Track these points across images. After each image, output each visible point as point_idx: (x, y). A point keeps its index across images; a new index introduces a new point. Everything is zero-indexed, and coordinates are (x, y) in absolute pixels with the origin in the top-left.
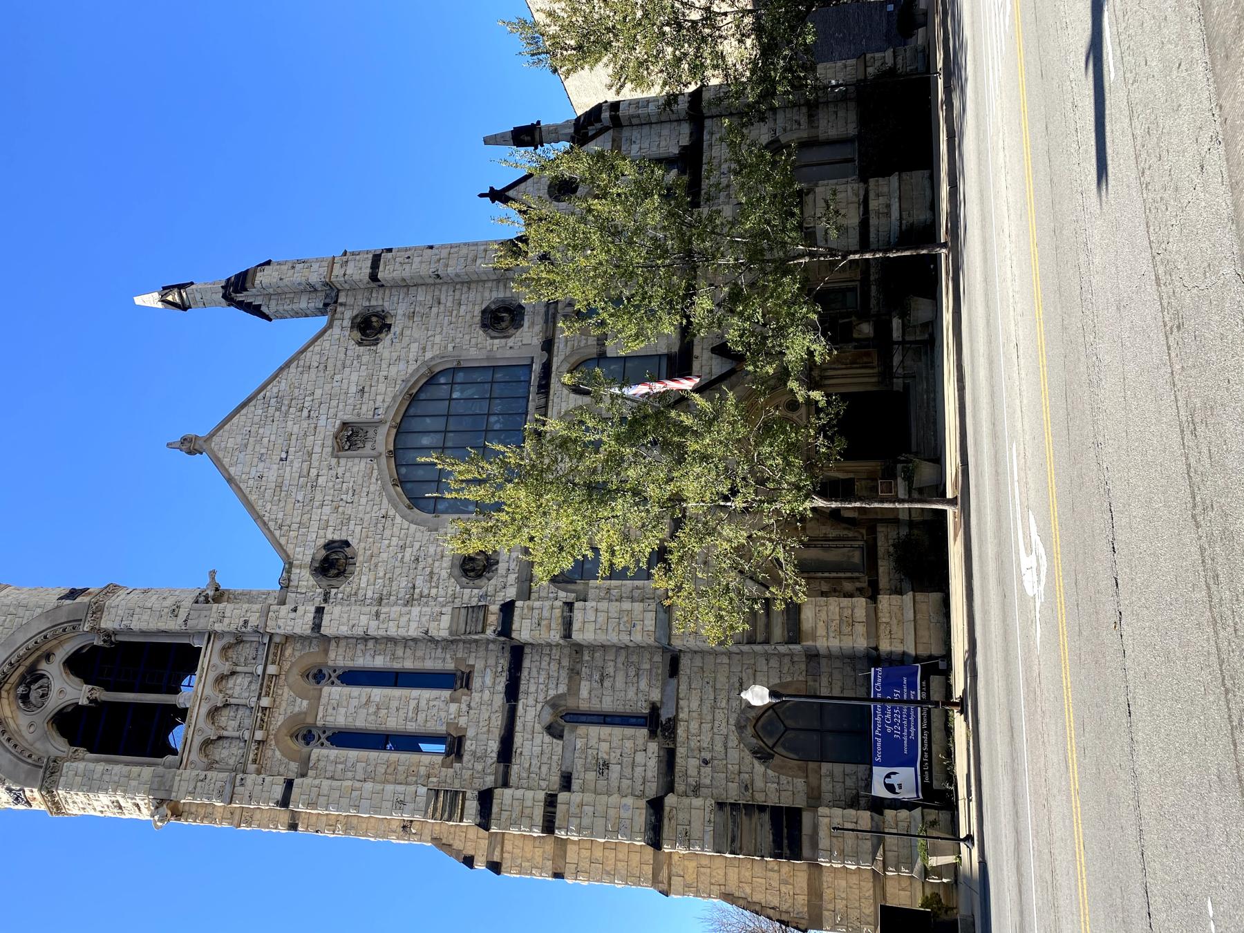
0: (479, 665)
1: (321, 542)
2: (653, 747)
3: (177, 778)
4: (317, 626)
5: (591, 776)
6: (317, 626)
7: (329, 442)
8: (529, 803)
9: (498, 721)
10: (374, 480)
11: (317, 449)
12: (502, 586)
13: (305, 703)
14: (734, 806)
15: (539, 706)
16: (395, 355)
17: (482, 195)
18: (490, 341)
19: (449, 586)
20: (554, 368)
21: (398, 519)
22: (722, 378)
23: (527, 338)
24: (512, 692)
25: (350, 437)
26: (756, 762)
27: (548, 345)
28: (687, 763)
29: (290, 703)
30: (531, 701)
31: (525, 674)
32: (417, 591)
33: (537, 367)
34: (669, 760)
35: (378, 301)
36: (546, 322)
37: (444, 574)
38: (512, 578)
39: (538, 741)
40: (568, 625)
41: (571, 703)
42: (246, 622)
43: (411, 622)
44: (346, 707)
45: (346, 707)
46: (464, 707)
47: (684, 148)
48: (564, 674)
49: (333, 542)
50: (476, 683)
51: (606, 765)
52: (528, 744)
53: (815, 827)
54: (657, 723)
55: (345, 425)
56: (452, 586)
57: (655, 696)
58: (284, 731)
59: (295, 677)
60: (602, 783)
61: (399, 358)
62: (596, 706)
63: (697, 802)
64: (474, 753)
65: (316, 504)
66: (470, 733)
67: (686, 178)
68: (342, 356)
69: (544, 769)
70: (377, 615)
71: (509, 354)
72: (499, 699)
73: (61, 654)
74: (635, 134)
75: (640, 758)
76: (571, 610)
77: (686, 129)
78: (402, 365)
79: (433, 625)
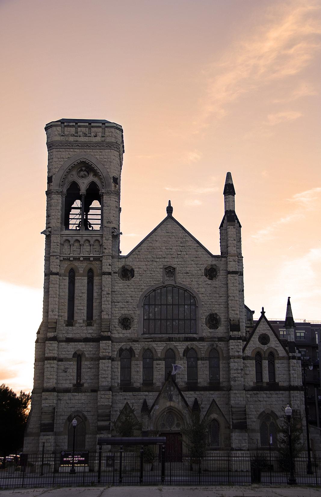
0: (94, 328)
1: (133, 267)
2: (71, 386)
3: (57, 236)
4: (104, 273)
5: (63, 367)
6: (104, 273)
7: (169, 264)
8: (53, 352)
9: (78, 336)
10: (155, 282)
11: (166, 260)
12: (118, 333)
13: (82, 272)
14: (54, 413)
15: (82, 349)
16: (200, 283)
17: (263, 308)
18: (205, 317)
19: (118, 313)
20: (194, 342)
21: (141, 293)
22: (185, 402)
23: (205, 331)
24: (86, 340)
25: (170, 271)
26: (67, 417)
27: (202, 339)
28: (66, 397)
29: (82, 267)
30: (84, 346)
31: (91, 343)
32: (117, 304)
33: (195, 335)
34: (67, 391)
35: (221, 274)
36: (211, 338)
37: (123, 312)
38: (121, 335)
39: (72, 350)
40: (104, 358)
41: (83, 359)
42: (106, 249)
43: (106, 306)
44: (81, 284)
45: (81, 284)
46: (82, 325)
47: (278, 384)
48: (91, 356)
49: (134, 271)
50: (89, 328)
51: (66, 372)
52: (71, 347)
53: (49, 435)
54: (78, 387)
55: (174, 269)
56: (118, 316)
57: (86, 385)
58: (73, 266)
59: (90, 266)
60: (61, 371)
61: (199, 285)
62: (83, 366)
63: (55, 401)
64: (68, 330)
65: (146, 263)
66: (74, 328)
67: (265, 385)
68: (201, 263)
69: (64, 353)
70: (108, 294)
71: (200, 325)
72: (84, 336)
73: (96, 180)
74: (285, 365)
75: (68, 382)
76: (108, 359)
77: (286, 384)
78: (196, 286)
79: (105, 313)
